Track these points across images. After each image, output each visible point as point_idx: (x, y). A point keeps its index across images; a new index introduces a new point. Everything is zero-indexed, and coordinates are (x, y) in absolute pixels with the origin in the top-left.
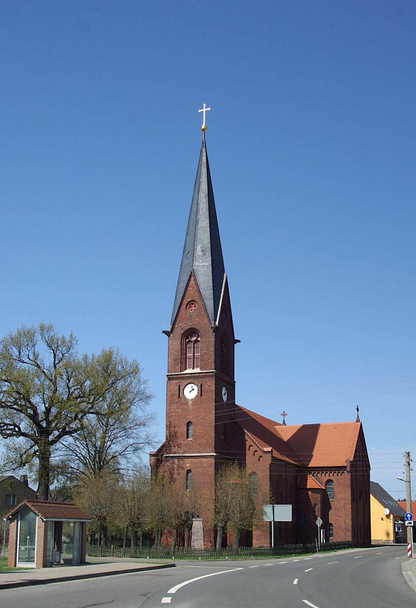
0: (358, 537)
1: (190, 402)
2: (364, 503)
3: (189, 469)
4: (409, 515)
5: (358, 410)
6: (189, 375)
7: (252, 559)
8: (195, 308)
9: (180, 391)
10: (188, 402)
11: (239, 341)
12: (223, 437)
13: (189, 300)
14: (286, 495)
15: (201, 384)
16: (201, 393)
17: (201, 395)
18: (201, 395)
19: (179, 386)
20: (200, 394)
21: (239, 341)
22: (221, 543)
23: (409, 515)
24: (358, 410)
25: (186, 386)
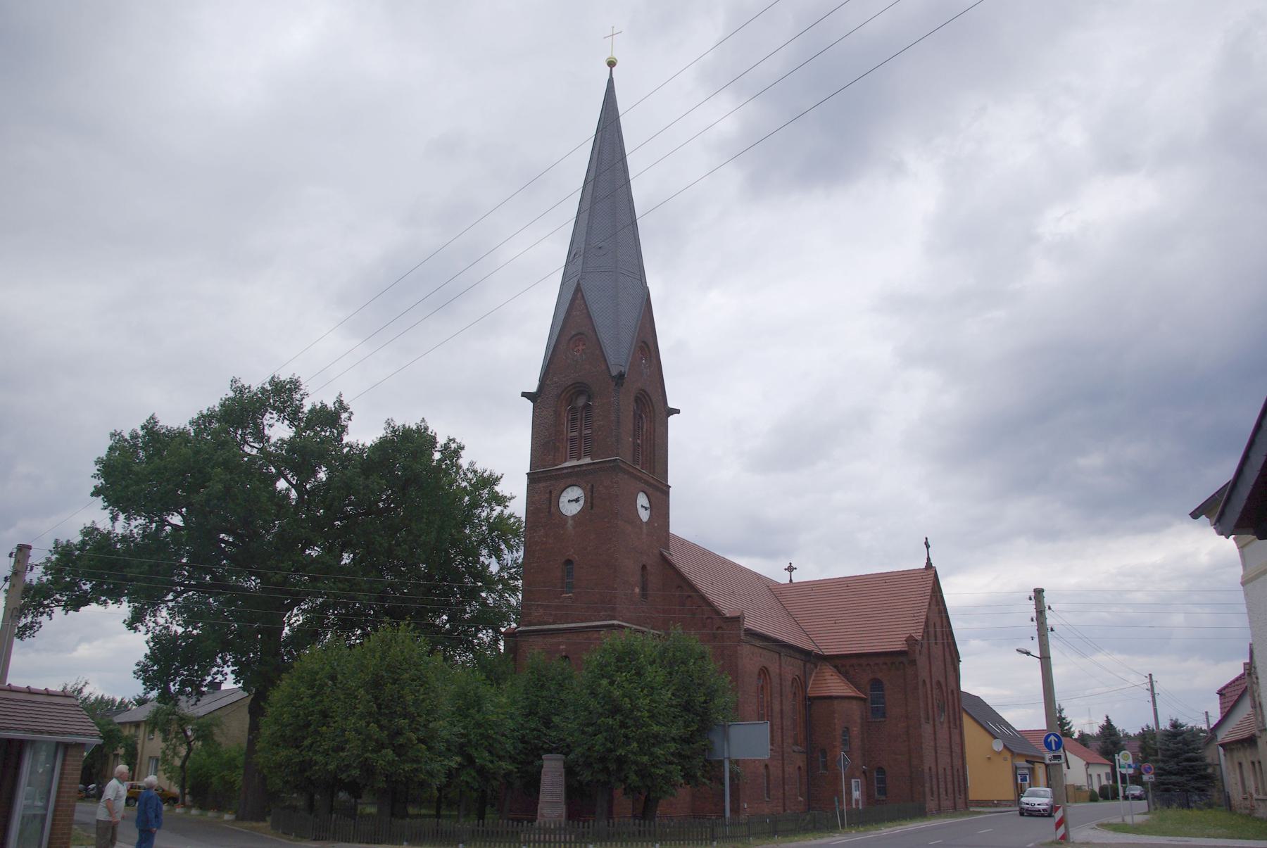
0: (939, 795)
1: (570, 522)
2: (950, 728)
3: (564, 654)
4: (1052, 738)
5: (927, 545)
6: (569, 470)
7: (291, 840)
8: (584, 347)
9: (553, 500)
10: (567, 522)
11: (677, 411)
12: (637, 590)
13: (573, 333)
14: (782, 710)
15: (592, 486)
16: (592, 503)
17: (592, 508)
18: (592, 508)
19: (550, 492)
20: (589, 504)
21: (677, 411)
22: (78, 742)
23: (1052, 738)
24: (927, 545)
25: (564, 490)
